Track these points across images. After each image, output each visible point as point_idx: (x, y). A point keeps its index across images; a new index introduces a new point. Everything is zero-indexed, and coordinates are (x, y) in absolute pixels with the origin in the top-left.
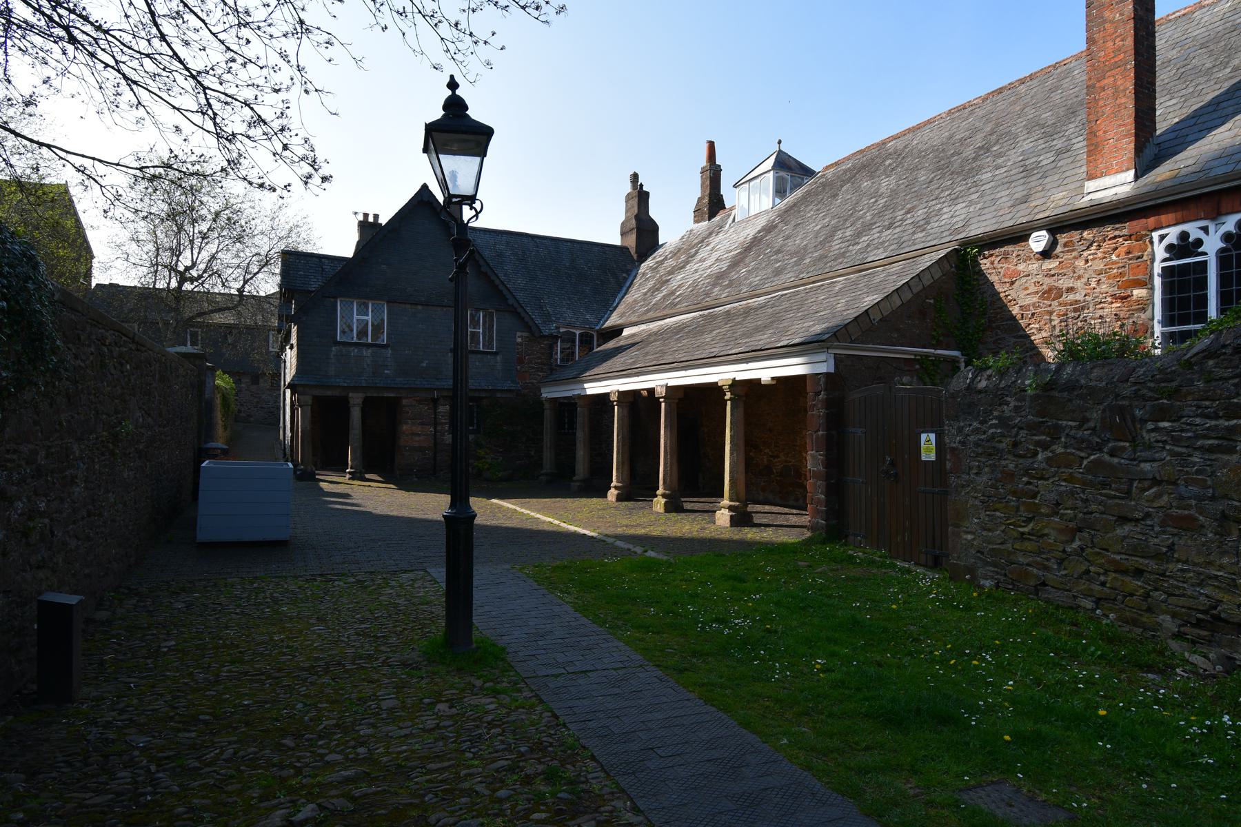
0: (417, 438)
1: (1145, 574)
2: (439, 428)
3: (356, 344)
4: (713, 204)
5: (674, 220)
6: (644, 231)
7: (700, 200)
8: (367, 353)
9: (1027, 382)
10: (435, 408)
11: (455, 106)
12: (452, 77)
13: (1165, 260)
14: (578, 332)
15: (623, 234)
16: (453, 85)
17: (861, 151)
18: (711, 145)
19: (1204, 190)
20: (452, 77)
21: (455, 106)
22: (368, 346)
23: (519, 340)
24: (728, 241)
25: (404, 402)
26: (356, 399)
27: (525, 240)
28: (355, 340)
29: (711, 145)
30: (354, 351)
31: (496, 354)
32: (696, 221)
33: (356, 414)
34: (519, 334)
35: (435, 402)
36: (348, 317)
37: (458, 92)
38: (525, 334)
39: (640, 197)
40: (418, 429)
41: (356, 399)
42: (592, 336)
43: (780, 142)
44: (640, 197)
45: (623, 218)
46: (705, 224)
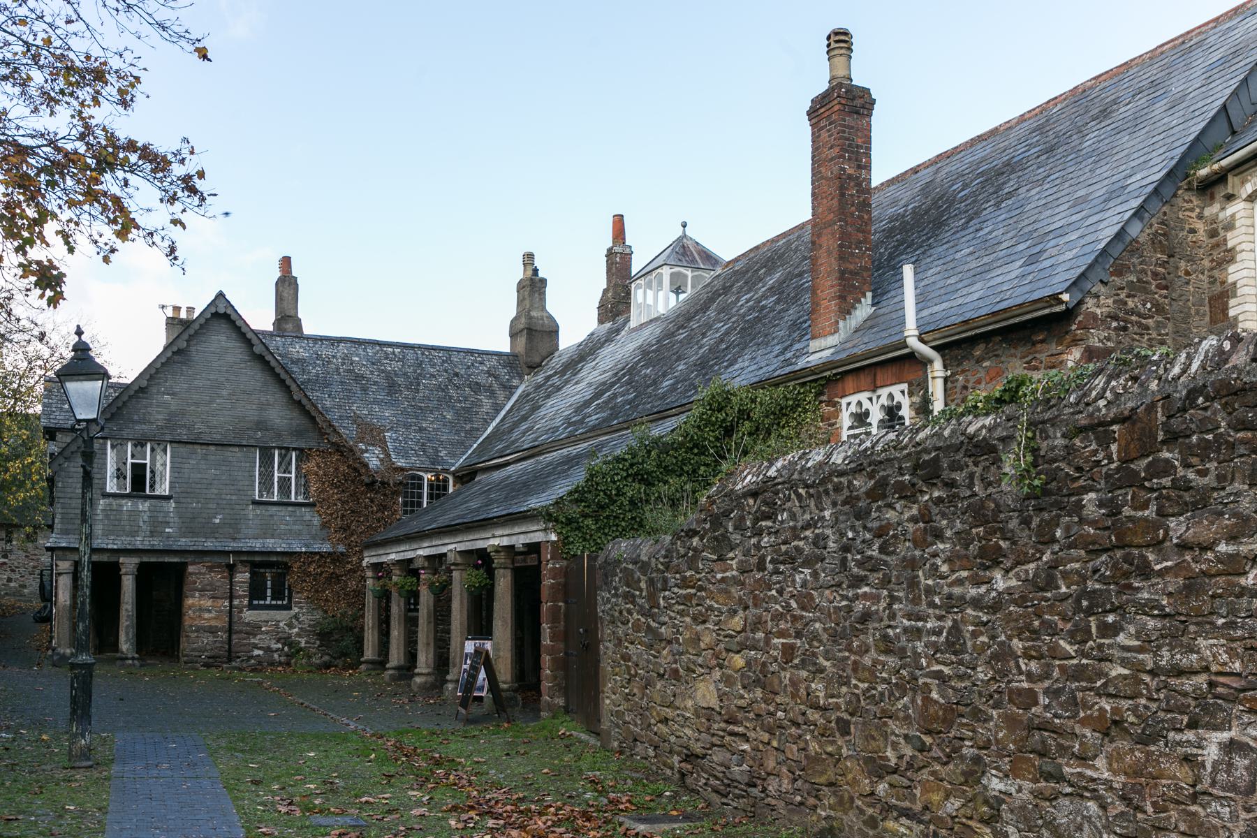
0: (207, 616)
2: (236, 602)
4: (615, 305)
5: (575, 320)
6: (534, 330)
7: (605, 292)
9: (550, 566)
10: (231, 576)
11: (82, 350)
12: (78, 326)
13: (850, 428)
15: (513, 335)
17: (757, 248)
18: (619, 222)
19: (863, 363)
20: (78, 326)
21: (82, 350)
24: (623, 349)
25: (191, 569)
26: (129, 565)
29: (619, 222)
32: (601, 321)
33: (269, 592)
35: (231, 569)
37: (84, 338)
40: (208, 603)
41: (129, 565)
43: (684, 225)
46: (608, 325)
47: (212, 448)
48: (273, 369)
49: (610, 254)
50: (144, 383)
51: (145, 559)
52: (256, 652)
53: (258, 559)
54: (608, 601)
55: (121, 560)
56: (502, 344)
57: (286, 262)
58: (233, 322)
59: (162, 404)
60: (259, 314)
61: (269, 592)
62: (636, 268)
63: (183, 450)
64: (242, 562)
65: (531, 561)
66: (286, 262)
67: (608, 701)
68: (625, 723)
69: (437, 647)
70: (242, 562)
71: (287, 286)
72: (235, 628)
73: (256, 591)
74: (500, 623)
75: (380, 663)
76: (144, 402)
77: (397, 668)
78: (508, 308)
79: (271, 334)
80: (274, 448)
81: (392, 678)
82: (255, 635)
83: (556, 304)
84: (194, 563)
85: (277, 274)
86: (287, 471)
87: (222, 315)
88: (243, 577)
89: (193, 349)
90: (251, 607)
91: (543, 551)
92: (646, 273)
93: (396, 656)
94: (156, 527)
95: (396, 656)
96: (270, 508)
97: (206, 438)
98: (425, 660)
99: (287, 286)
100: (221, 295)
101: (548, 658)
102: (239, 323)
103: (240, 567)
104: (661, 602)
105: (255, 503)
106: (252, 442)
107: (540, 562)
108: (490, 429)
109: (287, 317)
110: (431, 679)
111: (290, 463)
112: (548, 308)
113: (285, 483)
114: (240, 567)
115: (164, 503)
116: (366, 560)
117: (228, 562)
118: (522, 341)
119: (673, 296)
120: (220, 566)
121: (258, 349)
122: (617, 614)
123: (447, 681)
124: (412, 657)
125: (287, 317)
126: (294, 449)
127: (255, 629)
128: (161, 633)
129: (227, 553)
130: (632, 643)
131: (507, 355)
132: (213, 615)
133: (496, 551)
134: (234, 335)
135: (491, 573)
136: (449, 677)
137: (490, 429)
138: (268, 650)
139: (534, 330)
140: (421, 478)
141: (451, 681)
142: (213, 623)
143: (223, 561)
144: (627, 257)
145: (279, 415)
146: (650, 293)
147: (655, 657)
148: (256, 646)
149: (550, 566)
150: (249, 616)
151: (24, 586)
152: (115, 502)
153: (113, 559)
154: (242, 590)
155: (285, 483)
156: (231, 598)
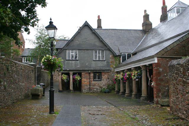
1: (23, 98)
2: (91, 80)
3: (75, 60)
5: (155, 21)
8: (73, 62)
11: (51, 23)
14: (127, 54)
16: (51, 19)
21: (51, 23)
22: (74, 60)
23: (111, 57)
25: (82, 73)
27: (113, 32)
28: (71, 59)
30: (71, 62)
31: (105, 61)
33: (97, 78)
34: (110, 55)
35: (90, 73)
36: (69, 53)
37: (52, 20)
38: (112, 55)
39: (146, 17)
40: (86, 80)
42: (131, 55)
44: (146, 17)
45: (143, 22)
47: (85, 50)
48: (96, 35)
49: (162, 8)
50: (73, 39)
51: (74, 72)
52: (95, 89)
53: (95, 71)
54: (171, 75)
55: (70, 72)
56: (141, 28)
57: (99, 17)
58: (89, 26)
59: (77, 42)
60: (94, 26)
61: (97, 78)
62: (168, 9)
63: (80, 51)
64: (92, 72)
65: (151, 68)
66: (99, 17)
67: (171, 99)
68: (177, 105)
69: (130, 88)
70: (92, 72)
71: (99, 21)
72: (91, 85)
73: (94, 77)
74: (143, 82)
75: (118, 92)
76: (73, 42)
77: (122, 92)
78: (142, 21)
79: (96, 29)
80: (97, 50)
81: (121, 94)
82: (95, 86)
83: (151, 19)
84: (83, 72)
85: (97, 19)
86: (100, 54)
87: (86, 25)
88: (92, 75)
89: (82, 32)
90: (94, 81)
91: (153, 65)
92: (170, 10)
93: (122, 90)
94: (76, 65)
95: (122, 90)
96: (97, 61)
97: (84, 49)
98: (127, 91)
99: (99, 21)
100: (86, 21)
101: (155, 89)
102: (90, 27)
103: (91, 73)
104: (187, 74)
105: (94, 61)
106: (93, 49)
107: (152, 68)
108: (139, 45)
109: (99, 26)
110: (129, 94)
111: (100, 53)
112: (150, 20)
113: (99, 57)
114: (91, 73)
115: (77, 61)
116: (115, 71)
117: (89, 72)
118: (145, 27)
119: (177, 14)
120: (88, 73)
121: (93, 31)
122: (174, 78)
123: (132, 95)
124: (125, 90)
125: (99, 26)
126: (101, 50)
127: (94, 85)
128: (78, 87)
129: (89, 70)
130: (178, 85)
131: (142, 30)
132: (87, 82)
133: (142, 66)
134: (89, 29)
135: (141, 71)
136: (133, 94)
137: (138, 45)
138: (97, 89)
139: (147, 27)
140: (126, 55)
141: (133, 95)
142: (87, 84)
143: (88, 72)
144: (166, 7)
145: (98, 44)
146: (172, 14)
147: (185, 88)
148: (95, 88)
149: (155, 68)
150: (93, 82)
151: (57, 79)
152: (68, 61)
153: (68, 72)
154: (92, 78)
155: (99, 57)
156: (90, 79)
